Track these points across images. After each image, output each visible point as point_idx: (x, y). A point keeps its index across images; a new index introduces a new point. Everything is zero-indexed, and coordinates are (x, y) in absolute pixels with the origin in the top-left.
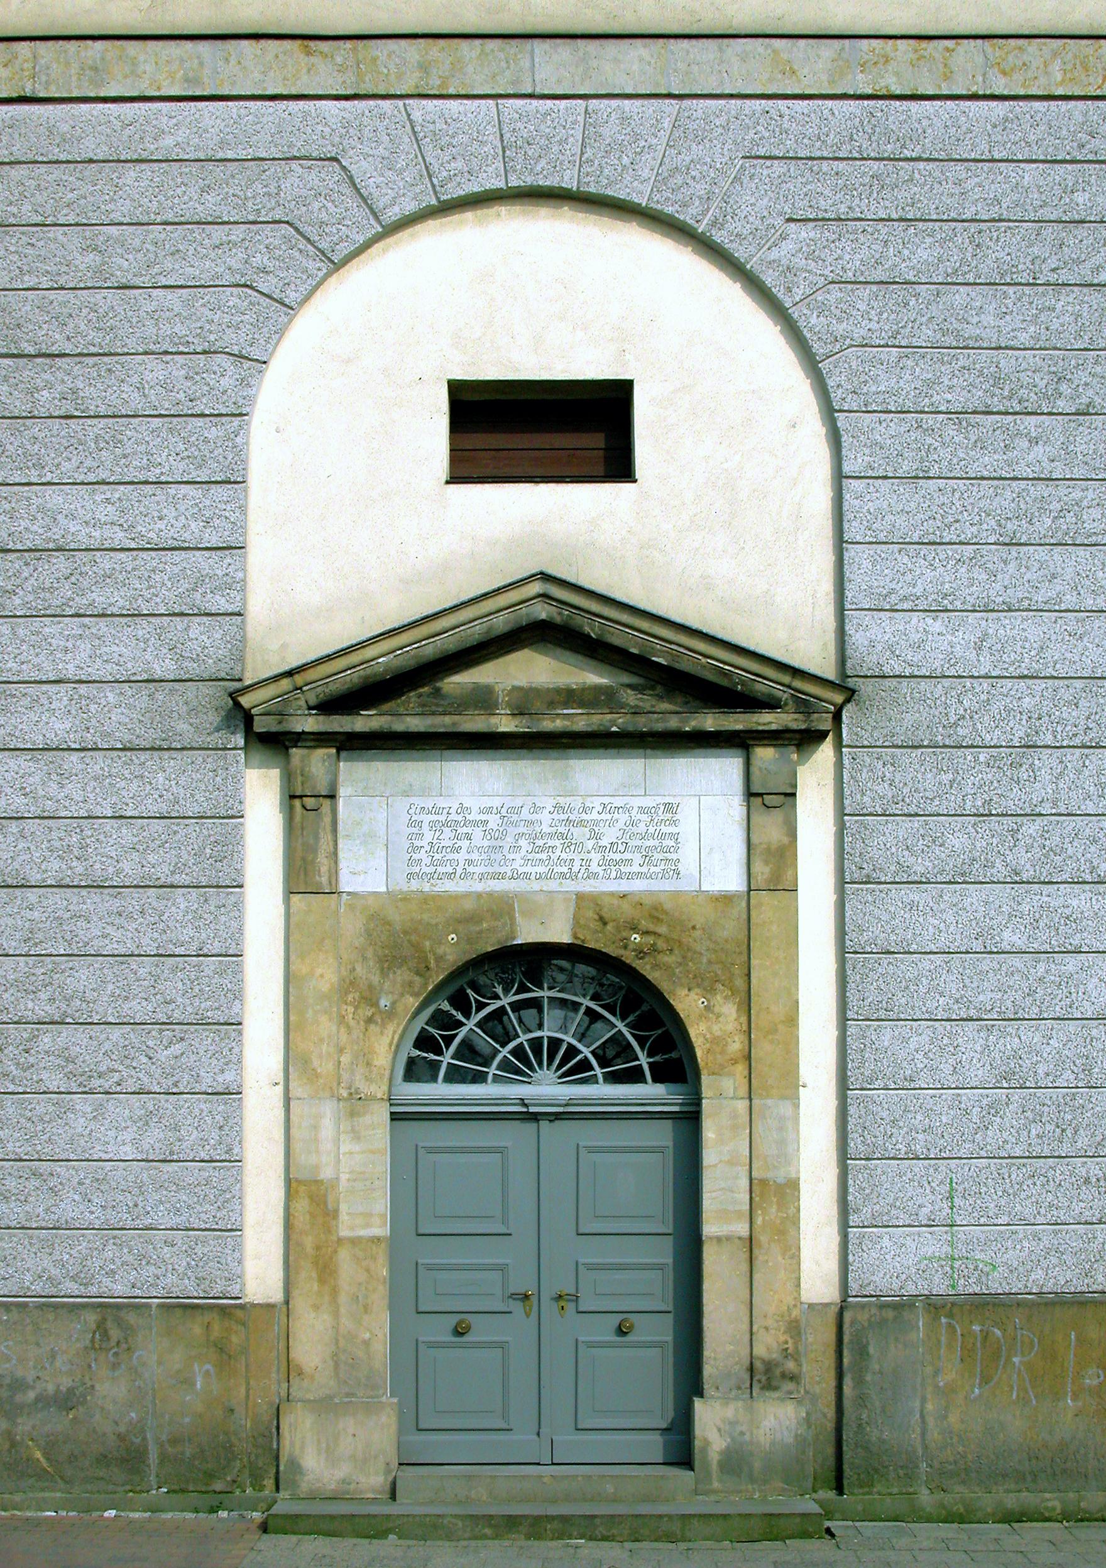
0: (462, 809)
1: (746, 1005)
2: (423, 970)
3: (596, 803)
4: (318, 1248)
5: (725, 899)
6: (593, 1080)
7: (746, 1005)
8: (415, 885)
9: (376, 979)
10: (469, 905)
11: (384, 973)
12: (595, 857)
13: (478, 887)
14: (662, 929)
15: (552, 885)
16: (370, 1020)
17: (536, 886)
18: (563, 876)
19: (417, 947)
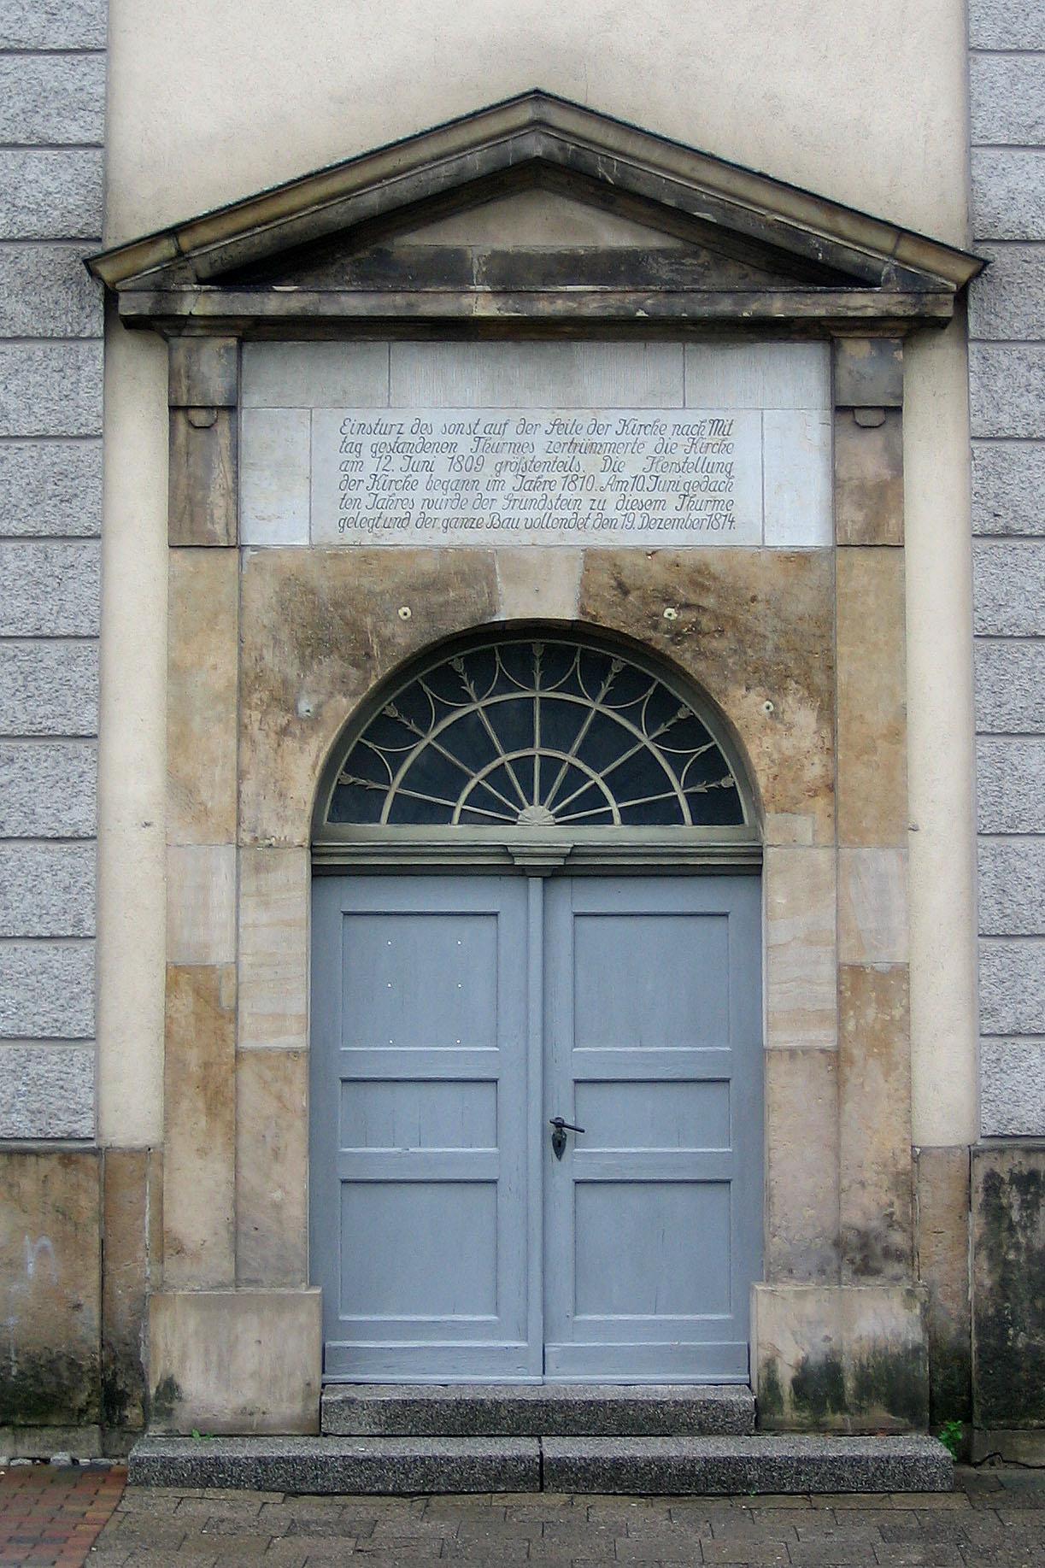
0: (420, 428)
1: (828, 711)
2: (361, 658)
3: (613, 418)
4: (207, 1065)
5: (800, 559)
6: (607, 818)
7: (828, 711)
8: (350, 536)
9: (292, 672)
10: (428, 565)
11: (304, 664)
12: (612, 496)
13: (442, 539)
14: (709, 601)
15: (550, 537)
16: (284, 731)
17: (526, 538)
18: (564, 523)
19: (353, 626)
